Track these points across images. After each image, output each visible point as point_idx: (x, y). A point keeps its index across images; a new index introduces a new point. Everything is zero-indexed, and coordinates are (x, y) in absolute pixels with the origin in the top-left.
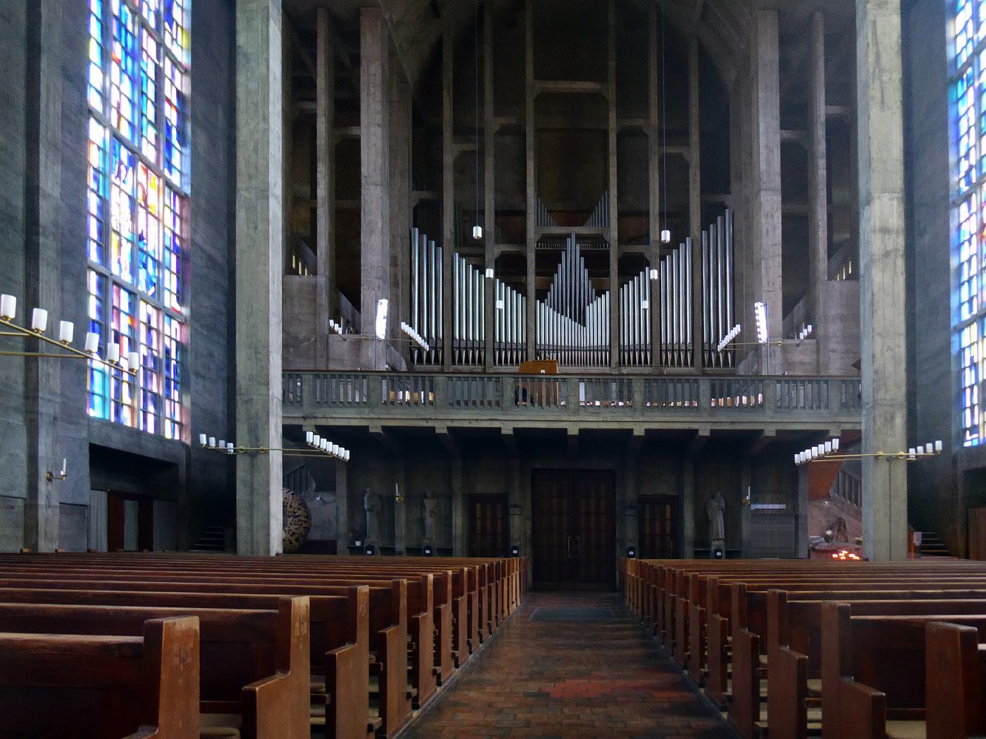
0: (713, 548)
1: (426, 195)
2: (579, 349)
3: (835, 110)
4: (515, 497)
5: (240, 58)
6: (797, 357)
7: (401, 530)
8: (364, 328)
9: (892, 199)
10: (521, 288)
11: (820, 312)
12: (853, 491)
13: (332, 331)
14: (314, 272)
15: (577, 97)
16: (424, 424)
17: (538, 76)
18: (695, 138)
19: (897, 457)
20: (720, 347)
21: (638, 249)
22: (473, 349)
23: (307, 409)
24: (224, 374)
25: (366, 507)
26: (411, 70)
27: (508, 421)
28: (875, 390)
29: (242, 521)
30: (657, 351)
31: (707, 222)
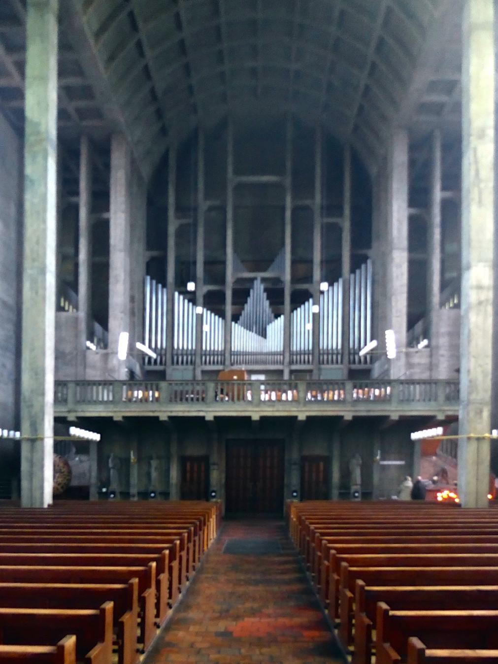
0: (352, 491)
1: (155, 253)
2: (261, 354)
3: (448, 194)
4: (214, 458)
5: (27, 183)
6: (416, 360)
7: (134, 479)
8: (111, 346)
9: (485, 267)
10: (221, 314)
11: (434, 330)
12: (452, 448)
13: (88, 348)
14: (76, 307)
15: (264, 186)
16: (151, 414)
17: (237, 172)
18: (347, 211)
19: (484, 438)
20: (362, 353)
21: (305, 286)
22: (187, 355)
23: (70, 405)
24: (13, 377)
25: (110, 465)
26: (146, 171)
27: (210, 412)
28: (469, 393)
29: (25, 484)
30: (317, 354)
31: (354, 268)
